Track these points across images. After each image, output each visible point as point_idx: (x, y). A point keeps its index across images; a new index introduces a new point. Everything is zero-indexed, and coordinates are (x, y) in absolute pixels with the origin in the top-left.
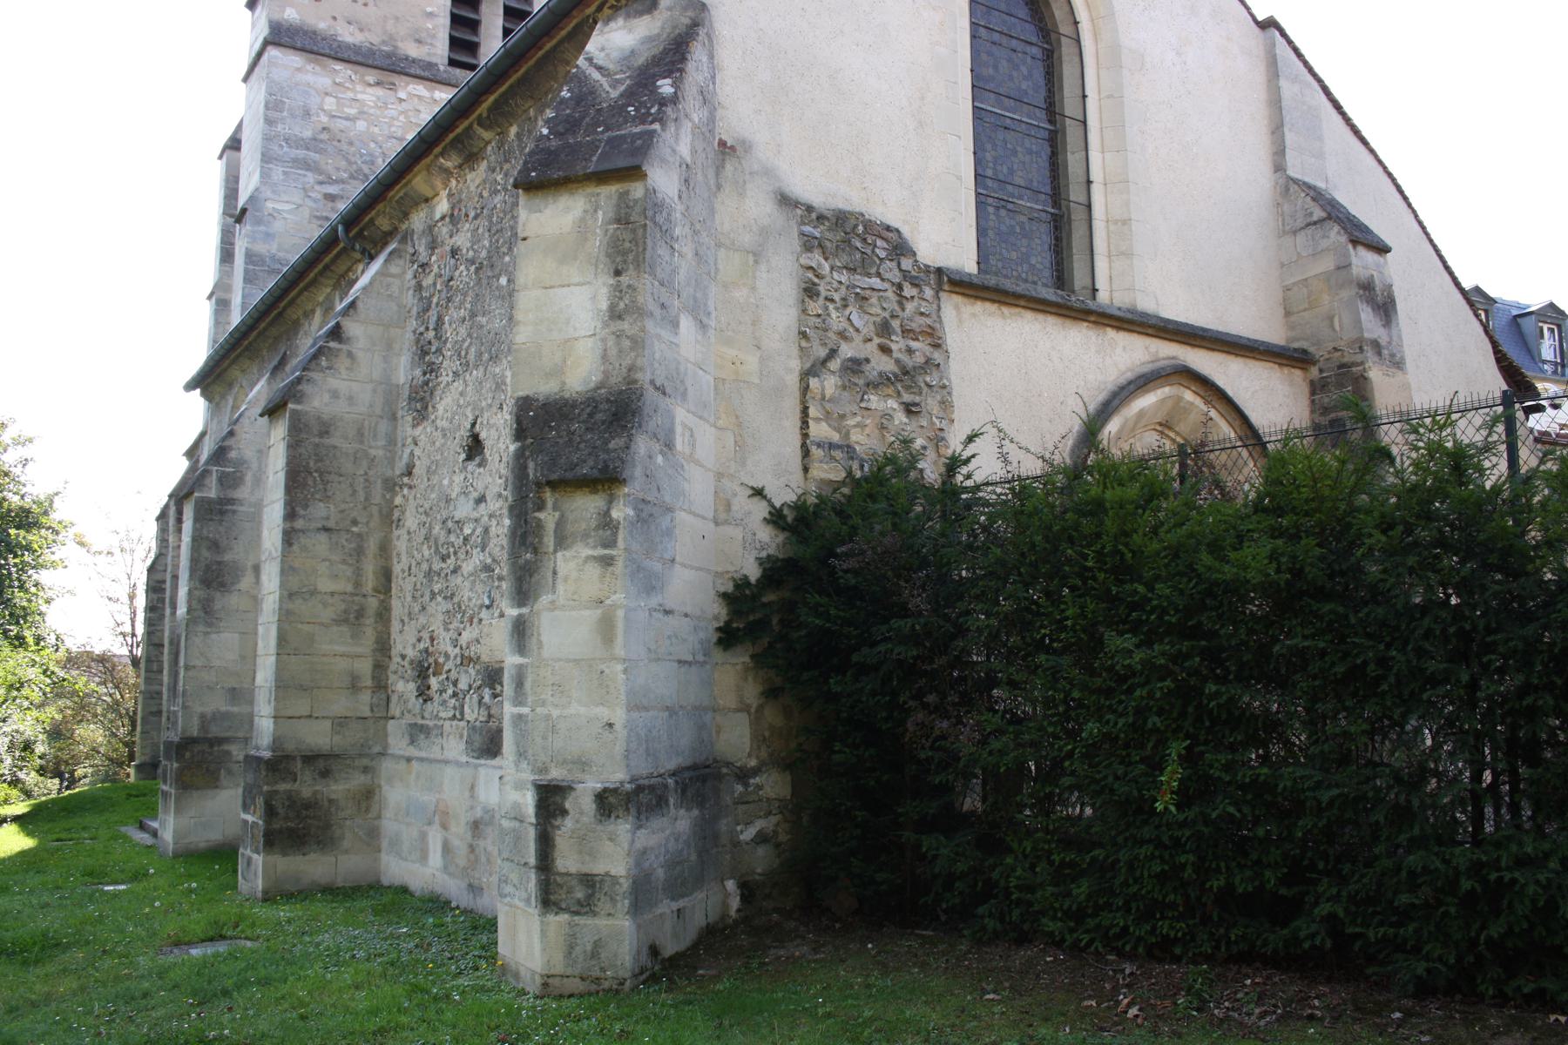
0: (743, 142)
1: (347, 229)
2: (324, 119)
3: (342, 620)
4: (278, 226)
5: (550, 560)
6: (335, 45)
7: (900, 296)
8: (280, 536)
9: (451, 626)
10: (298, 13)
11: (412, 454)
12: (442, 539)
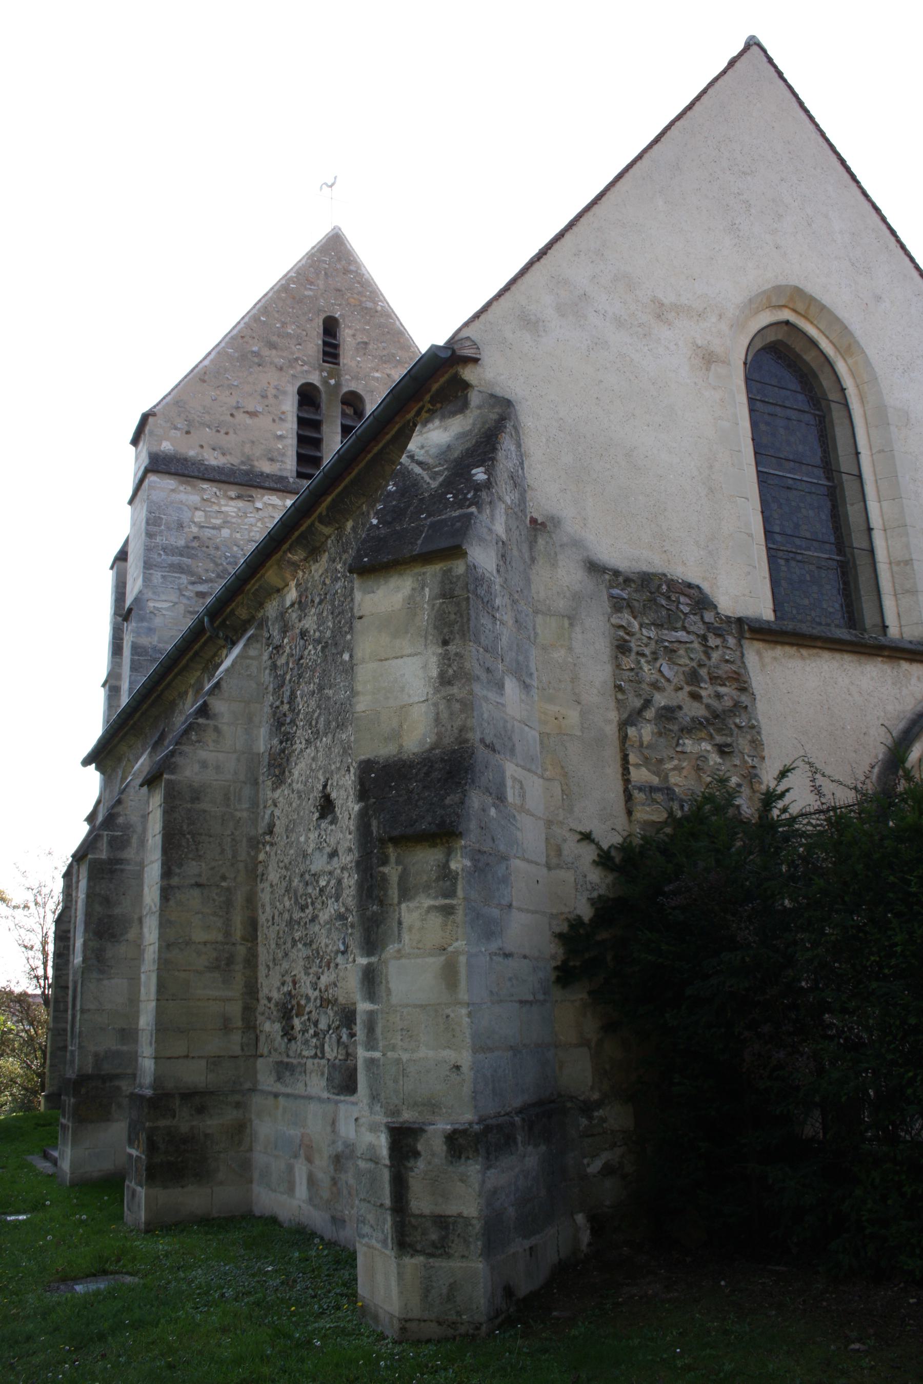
0: (552, 518)
1: (212, 621)
2: (195, 529)
3: (214, 967)
4: (158, 621)
5: (394, 911)
6: (202, 468)
7: (706, 646)
8: (159, 892)
9: (311, 971)
10: (172, 445)
11: (272, 814)
12: (301, 891)
